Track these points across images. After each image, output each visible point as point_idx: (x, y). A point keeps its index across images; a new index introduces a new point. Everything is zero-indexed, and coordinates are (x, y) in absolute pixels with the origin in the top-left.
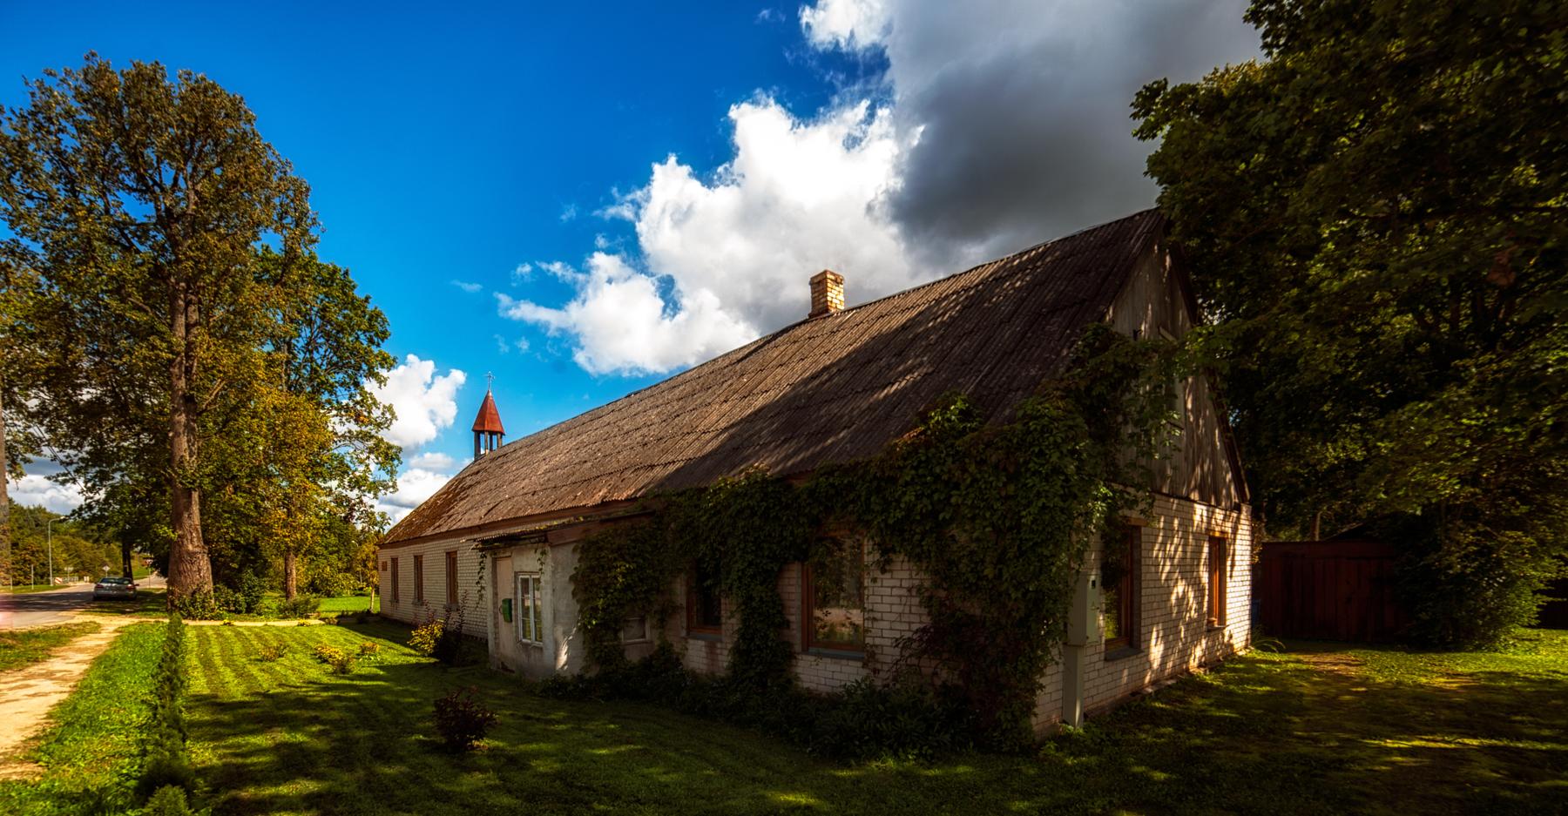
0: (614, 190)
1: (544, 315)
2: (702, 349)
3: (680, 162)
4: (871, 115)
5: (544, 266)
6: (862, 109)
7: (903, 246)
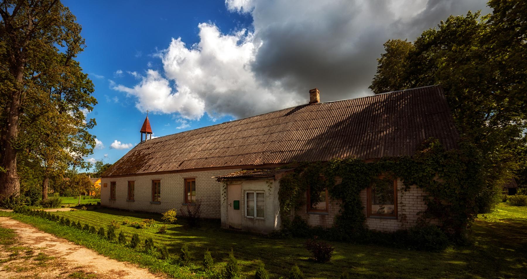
0: (156, 48)
1: (127, 90)
2: (183, 107)
3: (182, 40)
4: (246, 34)
5: (129, 72)
6: (243, 32)
7: (255, 79)
